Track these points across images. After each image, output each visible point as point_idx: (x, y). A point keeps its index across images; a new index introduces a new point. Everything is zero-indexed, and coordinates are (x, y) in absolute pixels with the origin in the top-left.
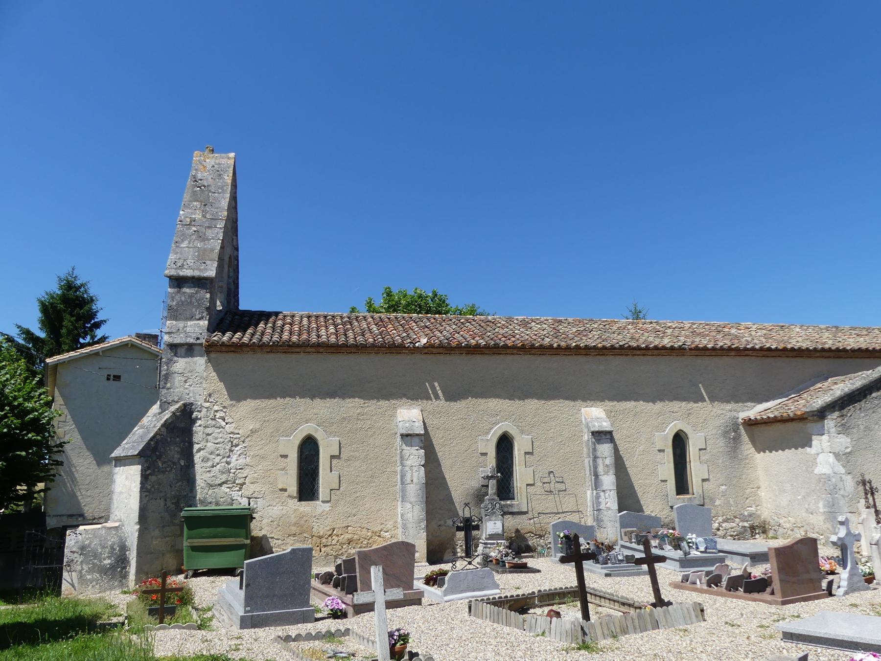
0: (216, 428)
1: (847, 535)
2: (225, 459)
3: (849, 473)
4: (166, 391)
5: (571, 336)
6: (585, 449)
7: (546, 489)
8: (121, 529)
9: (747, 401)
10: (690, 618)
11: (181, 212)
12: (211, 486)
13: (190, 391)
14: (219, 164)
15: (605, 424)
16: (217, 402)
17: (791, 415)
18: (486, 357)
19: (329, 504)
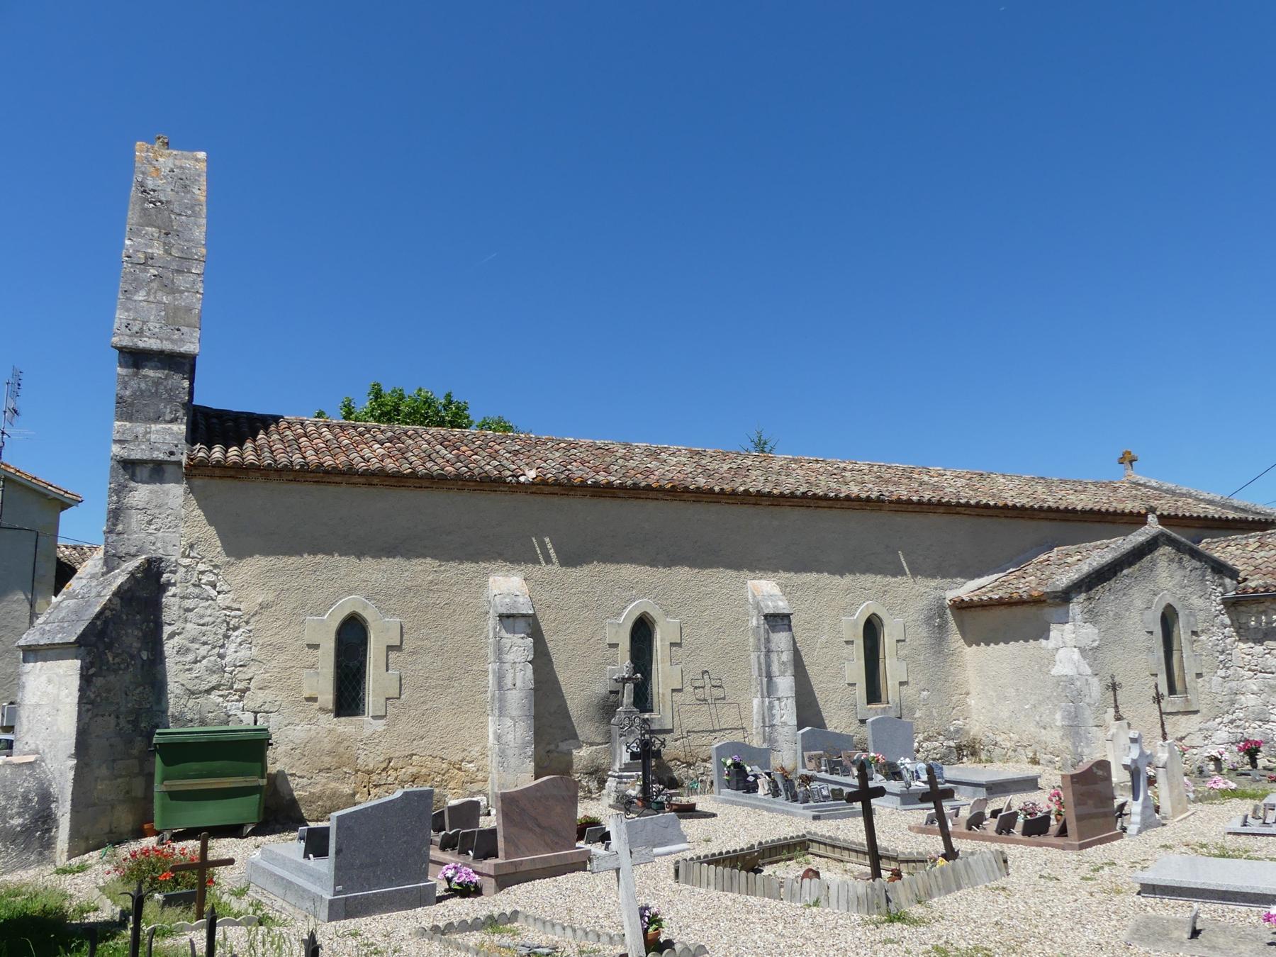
0: (202, 599)
1: (1140, 756)
2: (216, 650)
3: (1096, 675)
4: (115, 538)
5: (825, 486)
6: (751, 640)
7: (698, 697)
8: (40, 765)
10: (993, 871)
11: (128, 242)
12: (193, 693)
13: (156, 538)
14: (181, 167)
15: (781, 604)
16: (203, 558)
17: (1025, 596)
18: (618, 501)
19: (383, 721)
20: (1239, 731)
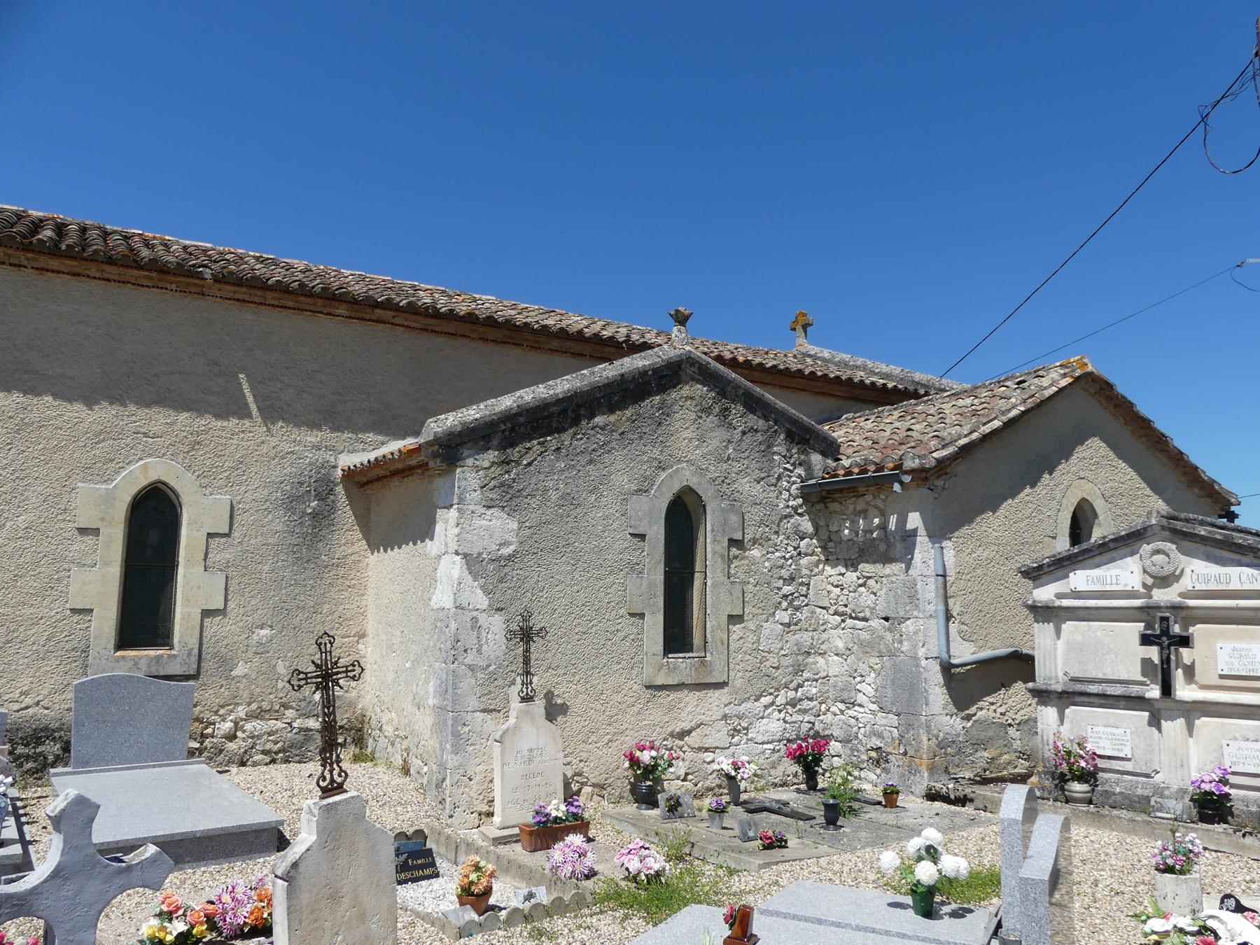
9: (366, 430)
20: (807, 719)
